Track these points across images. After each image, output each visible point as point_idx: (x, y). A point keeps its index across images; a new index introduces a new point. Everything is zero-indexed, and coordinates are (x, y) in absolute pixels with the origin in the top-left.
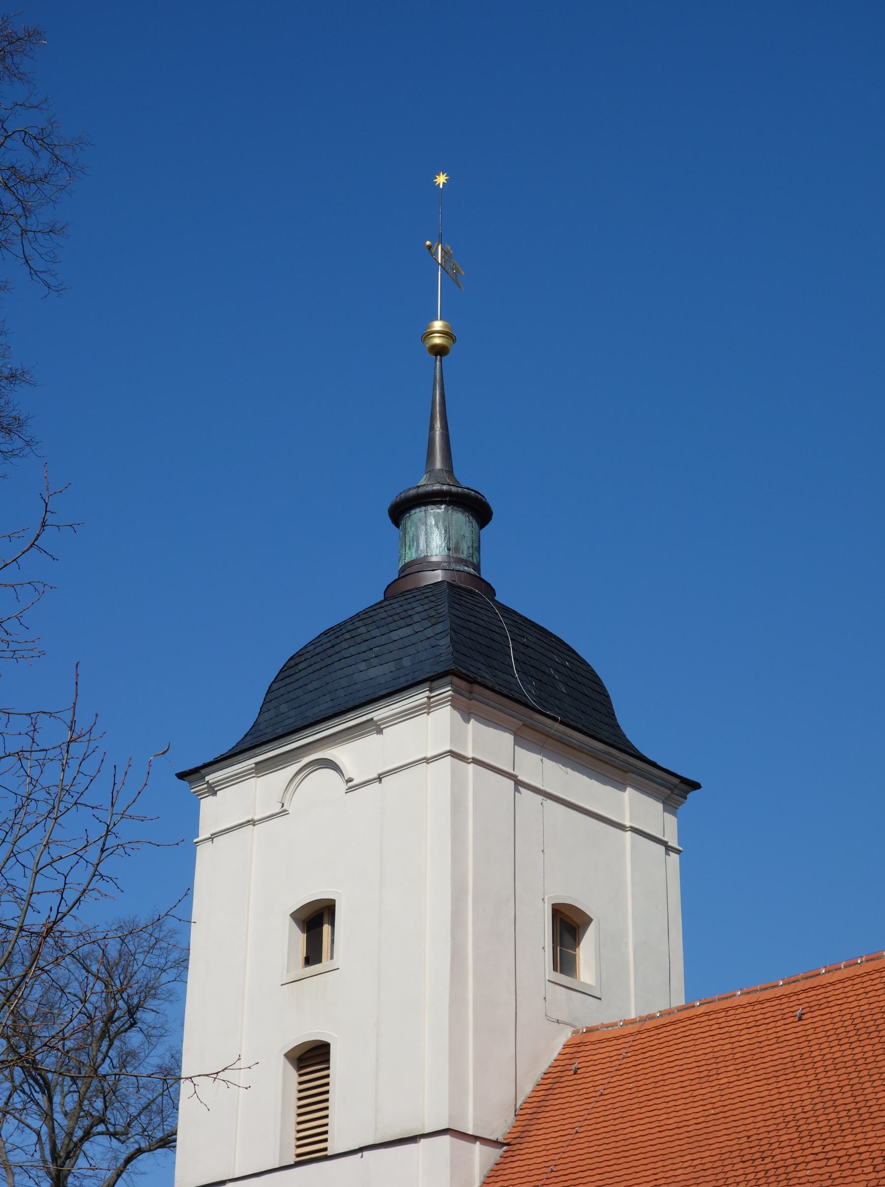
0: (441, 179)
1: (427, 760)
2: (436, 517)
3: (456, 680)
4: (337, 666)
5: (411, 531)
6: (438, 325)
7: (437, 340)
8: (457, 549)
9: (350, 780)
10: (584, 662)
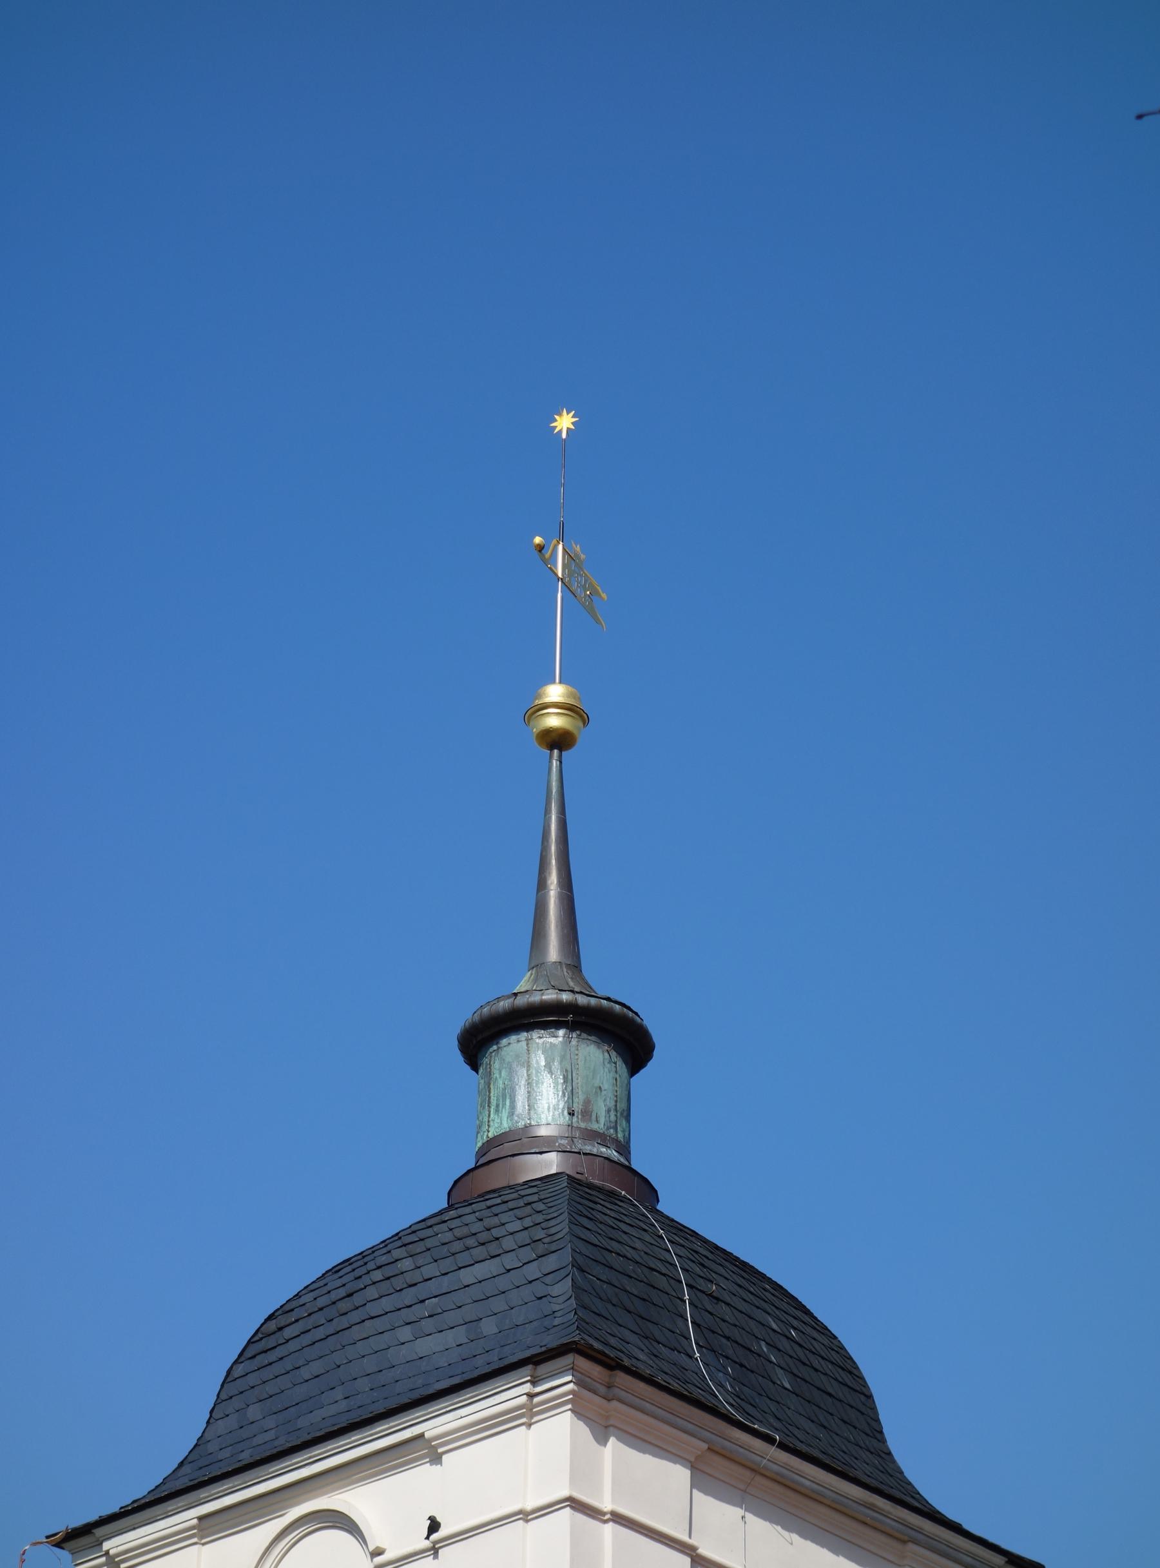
0: (564, 422)
1: (525, 1516)
2: (548, 1051)
3: (583, 1363)
4: (356, 1333)
5: (500, 1078)
6: (555, 692)
7: (554, 721)
8: (586, 1113)
9: (378, 1552)
10: (824, 1330)
